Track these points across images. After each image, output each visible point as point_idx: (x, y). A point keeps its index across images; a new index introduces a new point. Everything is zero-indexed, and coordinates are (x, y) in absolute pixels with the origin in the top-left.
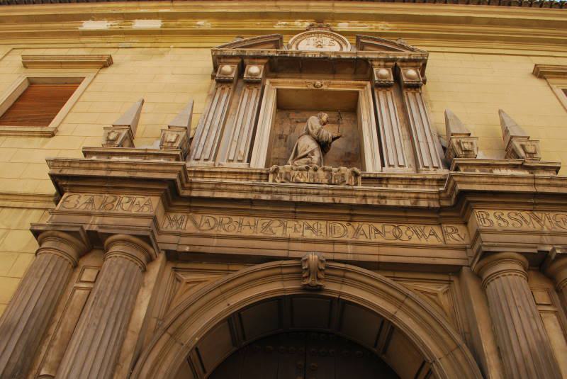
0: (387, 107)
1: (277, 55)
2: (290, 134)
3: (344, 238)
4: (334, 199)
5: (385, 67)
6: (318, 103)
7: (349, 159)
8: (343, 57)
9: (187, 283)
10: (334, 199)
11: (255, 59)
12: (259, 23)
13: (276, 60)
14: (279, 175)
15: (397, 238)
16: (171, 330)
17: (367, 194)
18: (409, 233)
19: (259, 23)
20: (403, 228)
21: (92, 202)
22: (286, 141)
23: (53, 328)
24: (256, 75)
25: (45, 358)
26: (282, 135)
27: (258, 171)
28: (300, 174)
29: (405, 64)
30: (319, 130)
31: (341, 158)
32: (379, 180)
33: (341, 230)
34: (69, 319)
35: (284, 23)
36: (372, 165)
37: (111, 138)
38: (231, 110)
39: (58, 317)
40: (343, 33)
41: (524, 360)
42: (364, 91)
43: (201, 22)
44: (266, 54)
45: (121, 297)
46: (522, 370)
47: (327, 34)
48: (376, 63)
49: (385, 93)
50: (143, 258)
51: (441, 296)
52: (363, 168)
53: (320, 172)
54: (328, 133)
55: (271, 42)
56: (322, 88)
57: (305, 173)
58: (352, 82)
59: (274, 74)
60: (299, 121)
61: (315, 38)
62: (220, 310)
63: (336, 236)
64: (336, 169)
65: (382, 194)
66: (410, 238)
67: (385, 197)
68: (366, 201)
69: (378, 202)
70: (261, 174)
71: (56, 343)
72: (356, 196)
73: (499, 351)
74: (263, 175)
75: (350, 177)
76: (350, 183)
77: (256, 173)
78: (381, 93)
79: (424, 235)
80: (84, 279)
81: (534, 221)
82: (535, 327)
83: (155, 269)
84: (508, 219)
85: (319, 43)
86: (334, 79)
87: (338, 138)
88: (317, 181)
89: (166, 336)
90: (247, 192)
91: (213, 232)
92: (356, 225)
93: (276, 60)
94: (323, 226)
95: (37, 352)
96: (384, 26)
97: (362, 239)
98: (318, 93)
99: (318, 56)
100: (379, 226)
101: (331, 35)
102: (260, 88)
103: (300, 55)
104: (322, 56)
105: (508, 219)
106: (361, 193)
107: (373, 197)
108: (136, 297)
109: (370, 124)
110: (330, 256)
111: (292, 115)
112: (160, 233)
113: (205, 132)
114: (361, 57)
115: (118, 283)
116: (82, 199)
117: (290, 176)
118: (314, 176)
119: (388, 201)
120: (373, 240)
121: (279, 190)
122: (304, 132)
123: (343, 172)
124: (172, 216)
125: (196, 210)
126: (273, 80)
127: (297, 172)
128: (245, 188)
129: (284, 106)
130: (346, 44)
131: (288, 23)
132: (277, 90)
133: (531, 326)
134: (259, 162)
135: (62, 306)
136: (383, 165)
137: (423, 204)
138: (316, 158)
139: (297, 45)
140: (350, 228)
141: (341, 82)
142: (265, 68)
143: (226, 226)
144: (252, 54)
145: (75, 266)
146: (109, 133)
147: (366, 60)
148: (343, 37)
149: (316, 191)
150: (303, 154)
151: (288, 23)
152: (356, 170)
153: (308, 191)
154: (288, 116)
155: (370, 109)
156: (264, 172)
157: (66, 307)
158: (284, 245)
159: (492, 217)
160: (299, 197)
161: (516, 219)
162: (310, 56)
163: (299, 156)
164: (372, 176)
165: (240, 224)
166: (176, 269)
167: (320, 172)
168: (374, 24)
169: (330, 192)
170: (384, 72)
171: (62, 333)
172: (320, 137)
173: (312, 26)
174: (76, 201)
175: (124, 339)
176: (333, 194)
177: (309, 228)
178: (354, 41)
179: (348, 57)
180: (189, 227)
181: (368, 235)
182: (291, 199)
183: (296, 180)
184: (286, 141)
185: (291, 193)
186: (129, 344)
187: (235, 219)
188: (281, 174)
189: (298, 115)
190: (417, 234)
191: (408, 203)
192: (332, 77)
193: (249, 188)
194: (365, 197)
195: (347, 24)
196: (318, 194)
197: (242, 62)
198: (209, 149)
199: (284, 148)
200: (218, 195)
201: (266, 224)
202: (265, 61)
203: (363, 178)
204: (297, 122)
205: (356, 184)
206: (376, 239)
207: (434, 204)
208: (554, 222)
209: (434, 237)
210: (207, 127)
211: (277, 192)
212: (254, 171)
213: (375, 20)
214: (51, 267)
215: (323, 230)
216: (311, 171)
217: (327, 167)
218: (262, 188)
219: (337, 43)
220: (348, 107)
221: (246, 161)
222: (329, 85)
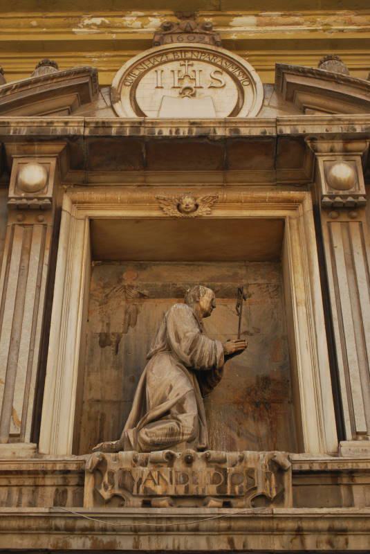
0: (351, 265)
1: (87, 132)
2: (126, 332)
4: (231, 542)
5: (347, 154)
6: (195, 245)
7: (267, 395)
8: (244, 131)
10: (231, 542)
11: (34, 142)
12: (34, 23)
13: (84, 145)
14: (106, 479)
17: (305, 525)
19: (34, 23)
22: (117, 351)
24: (39, 188)
26: (107, 335)
27: (59, 467)
28: (155, 474)
30: (195, 341)
31: (249, 392)
32: (334, 477)
35: (98, 21)
36: (318, 441)
40: (239, 46)
42: (298, 219)
44: (59, 132)
47: (203, 51)
49: (346, 226)
52: (299, 446)
53: (199, 466)
54: (211, 348)
57: (166, 470)
58: (269, 194)
59: (80, 176)
60: (145, 292)
61: (175, 66)
64: (235, 455)
65: (337, 524)
67: (343, 532)
68: (302, 542)
69: (330, 543)
70: (66, 472)
72: (281, 531)
74: (71, 478)
75: (267, 477)
76: (267, 492)
77: (53, 472)
78: (336, 228)
85: (186, 83)
86: (225, 185)
87: (238, 352)
88: (193, 490)
90: (38, 532)
93: (84, 145)
96: (345, 24)
98: (188, 225)
99: (184, 132)
101: (216, 54)
102: (50, 223)
103: (143, 132)
104: (195, 131)
106: (291, 525)
107: (317, 531)
109: (310, 315)
111: (129, 277)
114: (287, 130)
117: (133, 479)
118: (185, 477)
119: (351, 539)
121: (110, 524)
122: (159, 346)
123: (249, 466)
126: (81, 195)
127: (146, 470)
128: (33, 523)
129: (106, 253)
130: (252, 82)
131: (107, 21)
132: (92, 221)
134: (58, 440)
136: (341, 436)
138: (188, 420)
139: (135, 86)
141: (243, 195)
142: (57, 163)
144: (24, 132)
147: (300, 139)
148: (243, 61)
149: (192, 524)
150: (157, 412)
151: (107, 21)
152: (280, 456)
153: (174, 524)
154: (120, 280)
155: (311, 273)
156: (73, 467)
160: (153, 538)
162: (166, 133)
163: (152, 414)
164: (316, 467)
167: (199, 466)
168: (319, 19)
169: (223, 524)
170: (343, 171)
172: (196, 359)
173: (167, 29)
176: (229, 529)
178: (271, 77)
179: (256, 132)
182: (137, 544)
183: (146, 489)
184: (117, 351)
185: (136, 531)
188: (111, 474)
189: (145, 274)
192: (218, 178)
193: (42, 523)
194: (299, 532)
195: (252, 19)
196: (196, 531)
199: (115, 373)
202: (58, 148)
203: (296, 474)
204: (142, 296)
205: (279, 500)
211: (104, 530)
212: (49, 467)
213: (323, 8)
216: (179, 465)
217: (213, 453)
218: (70, 522)
219: (231, 84)
220: (266, 250)
221: (28, 436)
222: (214, 203)
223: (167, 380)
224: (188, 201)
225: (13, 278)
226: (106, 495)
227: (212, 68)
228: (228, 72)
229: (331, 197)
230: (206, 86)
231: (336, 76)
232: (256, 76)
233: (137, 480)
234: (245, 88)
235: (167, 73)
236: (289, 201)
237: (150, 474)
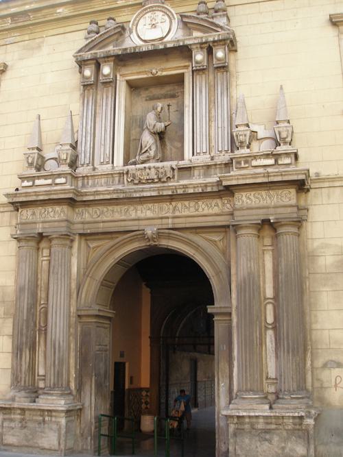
0: (201, 92)
3: (167, 215)
8: (169, 46)
9: (93, 248)
15: (197, 210)
16: (90, 275)
18: (203, 206)
20: (200, 203)
21: (34, 214)
23: (39, 282)
25: (41, 297)
29: (216, 44)
33: (166, 209)
34: (45, 276)
37: (30, 161)
38: (98, 108)
39: (39, 276)
43: (60, 10)
45: (63, 267)
48: (194, 47)
50: (68, 242)
51: (218, 243)
56: (157, 75)
59: (122, 63)
62: (111, 261)
71: (43, 289)
81: (268, 198)
82: (249, 265)
83: (76, 245)
85: (154, 22)
89: (89, 279)
91: (99, 219)
92: (174, 204)
94: (157, 207)
95: (37, 294)
97: (177, 214)
102: (114, 86)
103: (137, 50)
108: (70, 262)
110: (160, 227)
112: (73, 224)
113: (84, 139)
115: (60, 261)
120: (183, 213)
124: (77, 210)
125: (88, 206)
129: (133, 87)
133: (247, 265)
135: (39, 271)
137: (209, 189)
138: (152, 153)
140: (171, 206)
144: (102, 56)
145: (38, 249)
146: (28, 158)
157: (41, 270)
158: (136, 222)
159: (244, 198)
161: (257, 198)
166: (86, 240)
174: (26, 214)
175: (70, 283)
180: (87, 217)
186: (74, 286)
187: (110, 208)
190: (208, 206)
191: (200, 190)
197: (97, 61)
198: (89, 131)
200: (97, 198)
206: (188, 212)
207: (215, 189)
210: (84, 134)
214: (28, 255)
220: (179, 80)
223: (148, 139)
224: (154, 71)
225: (104, 108)
226: (129, 180)
227: (162, 13)
229: (196, 67)
232: (175, 15)
235: (147, 18)
236: (185, 66)
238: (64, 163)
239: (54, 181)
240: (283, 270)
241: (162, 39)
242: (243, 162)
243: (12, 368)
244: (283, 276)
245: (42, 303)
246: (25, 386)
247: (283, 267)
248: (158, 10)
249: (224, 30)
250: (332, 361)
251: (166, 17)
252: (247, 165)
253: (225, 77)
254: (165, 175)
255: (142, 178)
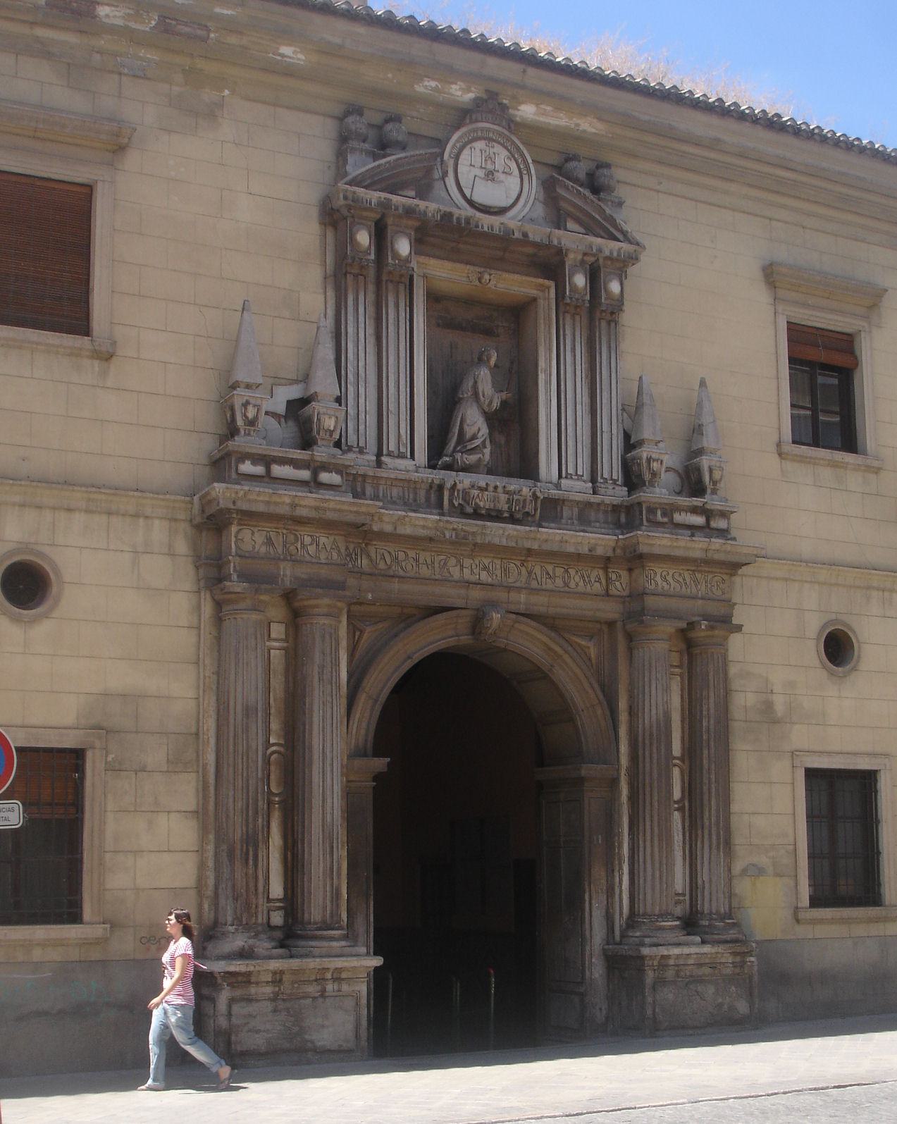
0: (573, 349)
18: (577, 579)
28: (480, 495)
41: (651, 727)
46: (647, 734)
55: (198, 729)
63: (510, 580)
66: (577, 585)
71: (273, 711)
73: (632, 712)
79: (590, 581)
80: (273, 635)
84: (671, 581)
85: (490, 166)
94: (498, 567)
100: (550, 568)
105: (671, 581)
116: (256, 534)
132: (414, 460)
143: (404, 564)
161: (678, 582)
165: (417, 561)
171: (275, 700)
177: (485, 568)
181: (539, 579)
183: (476, 504)
190: (584, 580)
201: (442, 563)
208: (709, 586)
209: (598, 584)
215: (498, 572)
228: (517, 163)
230: (414, 463)
231: (471, 369)
233: (472, 496)
234: (524, 176)
237: (478, 495)
238: (328, 436)
239: (315, 474)
240: (712, 711)
241: (502, 211)
242: (659, 513)
243: (200, 886)
244: (712, 722)
245: (272, 741)
246: (346, 937)
247: (712, 705)
248: (503, 145)
249: (631, 243)
250: (753, 865)
251: (513, 165)
252: (666, 520)
253: (613, 332)
254: (524, 507)
255: (482, 504)
